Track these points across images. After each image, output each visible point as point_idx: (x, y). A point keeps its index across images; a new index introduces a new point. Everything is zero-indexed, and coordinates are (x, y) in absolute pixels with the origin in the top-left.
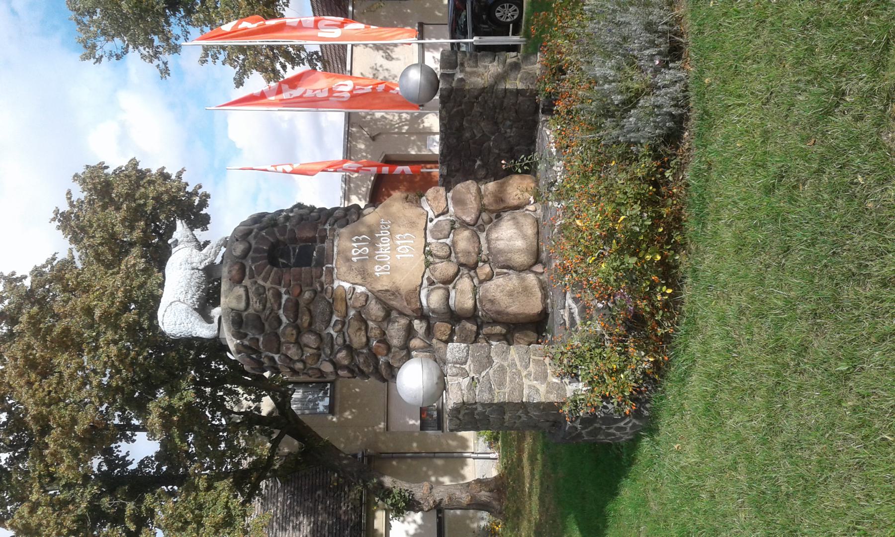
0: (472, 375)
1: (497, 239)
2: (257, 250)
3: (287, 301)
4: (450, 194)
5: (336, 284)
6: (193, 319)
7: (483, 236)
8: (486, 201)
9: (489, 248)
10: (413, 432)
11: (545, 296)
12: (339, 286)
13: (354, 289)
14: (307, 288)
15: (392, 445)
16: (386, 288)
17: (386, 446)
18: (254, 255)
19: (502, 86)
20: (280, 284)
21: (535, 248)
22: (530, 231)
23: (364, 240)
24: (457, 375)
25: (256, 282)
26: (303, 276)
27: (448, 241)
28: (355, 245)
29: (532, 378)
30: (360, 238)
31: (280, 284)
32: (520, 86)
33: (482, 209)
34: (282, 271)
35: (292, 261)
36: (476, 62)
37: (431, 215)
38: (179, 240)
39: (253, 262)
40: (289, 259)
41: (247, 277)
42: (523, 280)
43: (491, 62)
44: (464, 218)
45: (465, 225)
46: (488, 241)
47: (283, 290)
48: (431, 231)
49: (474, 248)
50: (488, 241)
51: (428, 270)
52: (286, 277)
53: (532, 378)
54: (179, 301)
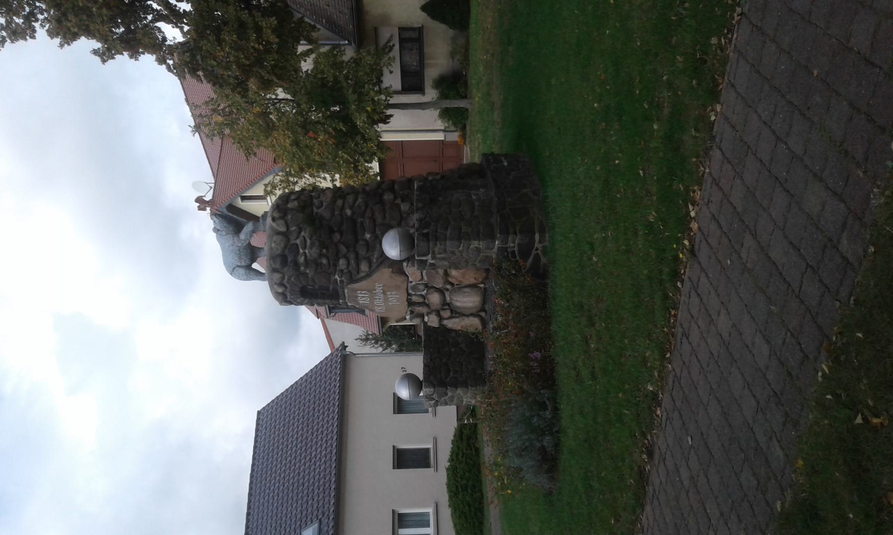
37: (410, 279)
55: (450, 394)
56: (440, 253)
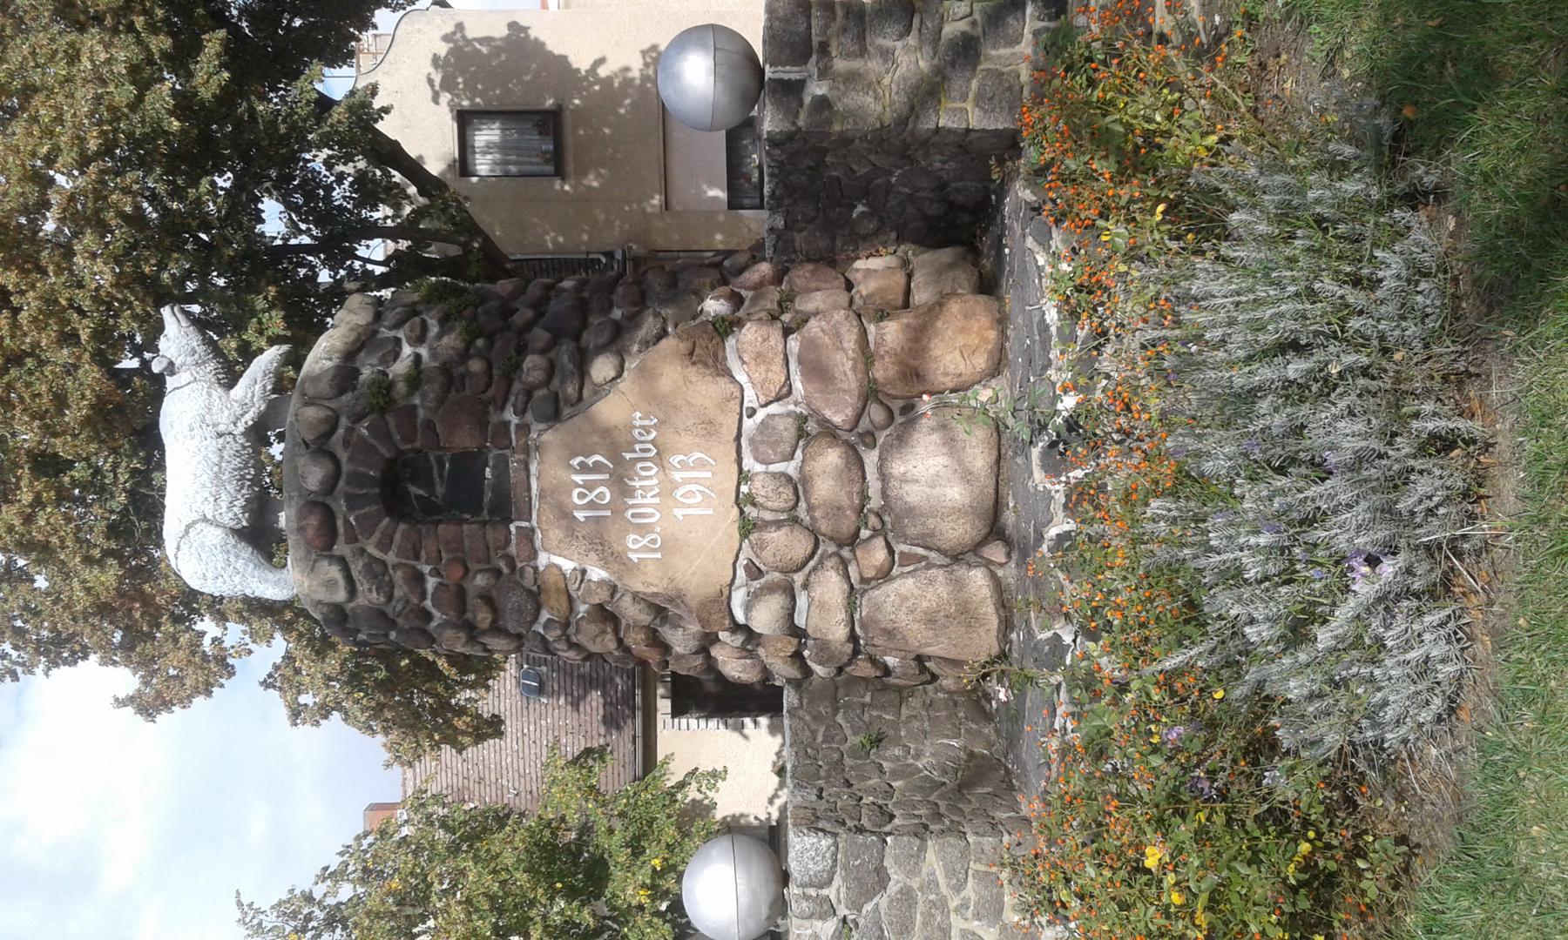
0: (842, 911)
1: (904, 480)
2: (355, 479)
3: (436, 589)
4: (794, 343)
5: (543, 559)
6: (240, 564)
7: (871, 458)
8: (881, 372)
9: (884, 494)
10: (718, 213)
11: (1007, 625)
12: (551, 565)
13: (584, 572)
14: (479, 566)
15: (676, 237)
16: (655, 590)
17: (668, 237)
18: (351, 490)
19: (927, 124)
20: (417, 558)
21: (990, 502)
22: (979, 459)
23: (597, 468)
24: (811, 917)
25: (363, 551)
26: (467, 543)
27: (791, 468)
28: (578, 478)
29: (969, 914)
30: (590, 461)
31: (417, 558)
32: (976, 119)
33: (871, 393)
34: (418, 532)
35: (440, 490)
36: (861, 38)
37: (750, 398)
38: (178, 363)
39: (351, 508)
40: (430, 485)
41: (341, 538)
42: (959, 585)
43: (901, 37)
44: (828, 413)
45: (830, 432)
46: (884, 477)
47: (426, 569)
48: (752, 441)
49: (850, 494)
50: (884, 477)
51: (746, 543)
52: (429, 547)
53: (969, 914)
54: (205, 519)
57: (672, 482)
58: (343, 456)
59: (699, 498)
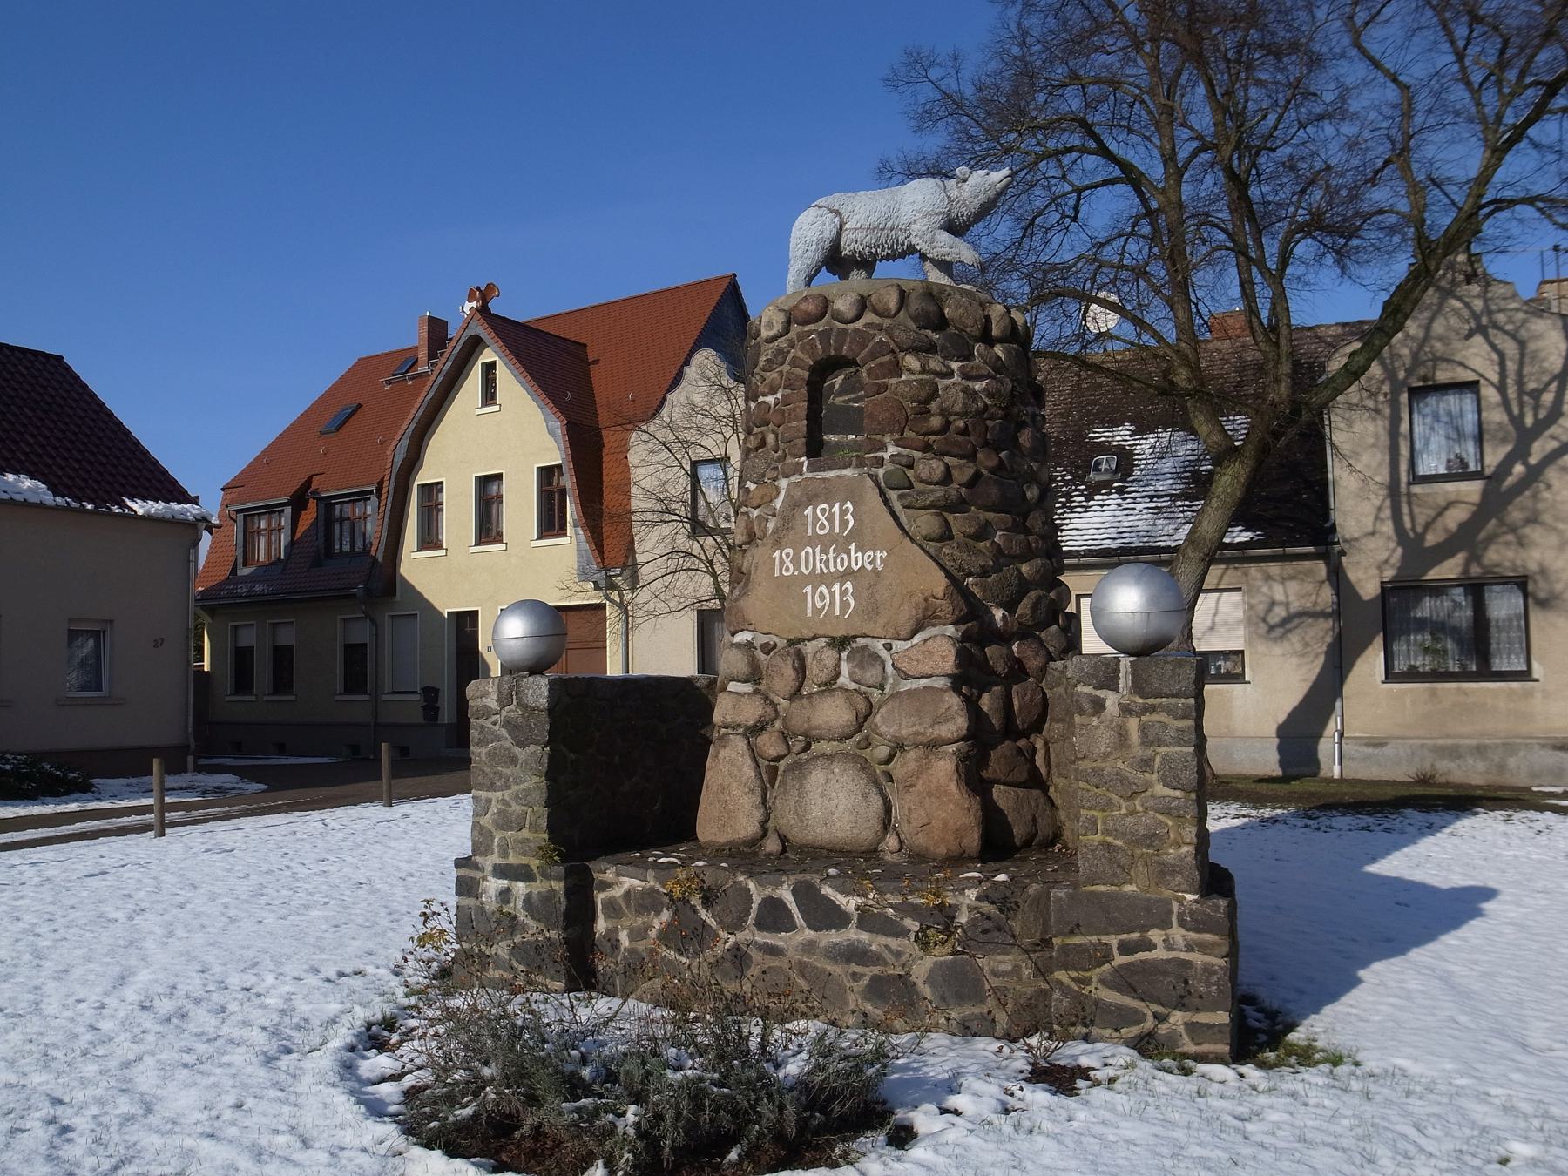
23: (844, 523)
30: (849, 516)
35: (839, 400)
37: (899, 646)
39: (820, 334)
40: (841, 393)
47: (779, 396)
55: (521, 753)
56: (1143, 729)
57: (832, 584)
58: (859, 324)
59: (819, 605)
